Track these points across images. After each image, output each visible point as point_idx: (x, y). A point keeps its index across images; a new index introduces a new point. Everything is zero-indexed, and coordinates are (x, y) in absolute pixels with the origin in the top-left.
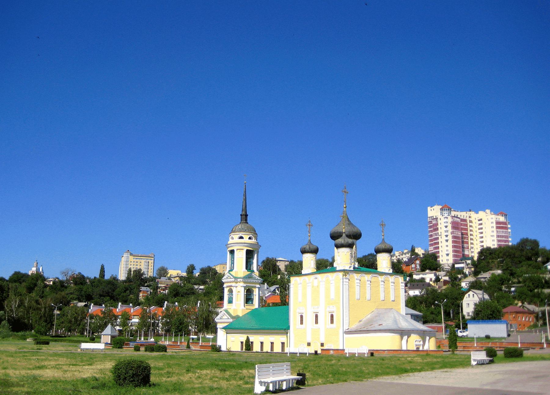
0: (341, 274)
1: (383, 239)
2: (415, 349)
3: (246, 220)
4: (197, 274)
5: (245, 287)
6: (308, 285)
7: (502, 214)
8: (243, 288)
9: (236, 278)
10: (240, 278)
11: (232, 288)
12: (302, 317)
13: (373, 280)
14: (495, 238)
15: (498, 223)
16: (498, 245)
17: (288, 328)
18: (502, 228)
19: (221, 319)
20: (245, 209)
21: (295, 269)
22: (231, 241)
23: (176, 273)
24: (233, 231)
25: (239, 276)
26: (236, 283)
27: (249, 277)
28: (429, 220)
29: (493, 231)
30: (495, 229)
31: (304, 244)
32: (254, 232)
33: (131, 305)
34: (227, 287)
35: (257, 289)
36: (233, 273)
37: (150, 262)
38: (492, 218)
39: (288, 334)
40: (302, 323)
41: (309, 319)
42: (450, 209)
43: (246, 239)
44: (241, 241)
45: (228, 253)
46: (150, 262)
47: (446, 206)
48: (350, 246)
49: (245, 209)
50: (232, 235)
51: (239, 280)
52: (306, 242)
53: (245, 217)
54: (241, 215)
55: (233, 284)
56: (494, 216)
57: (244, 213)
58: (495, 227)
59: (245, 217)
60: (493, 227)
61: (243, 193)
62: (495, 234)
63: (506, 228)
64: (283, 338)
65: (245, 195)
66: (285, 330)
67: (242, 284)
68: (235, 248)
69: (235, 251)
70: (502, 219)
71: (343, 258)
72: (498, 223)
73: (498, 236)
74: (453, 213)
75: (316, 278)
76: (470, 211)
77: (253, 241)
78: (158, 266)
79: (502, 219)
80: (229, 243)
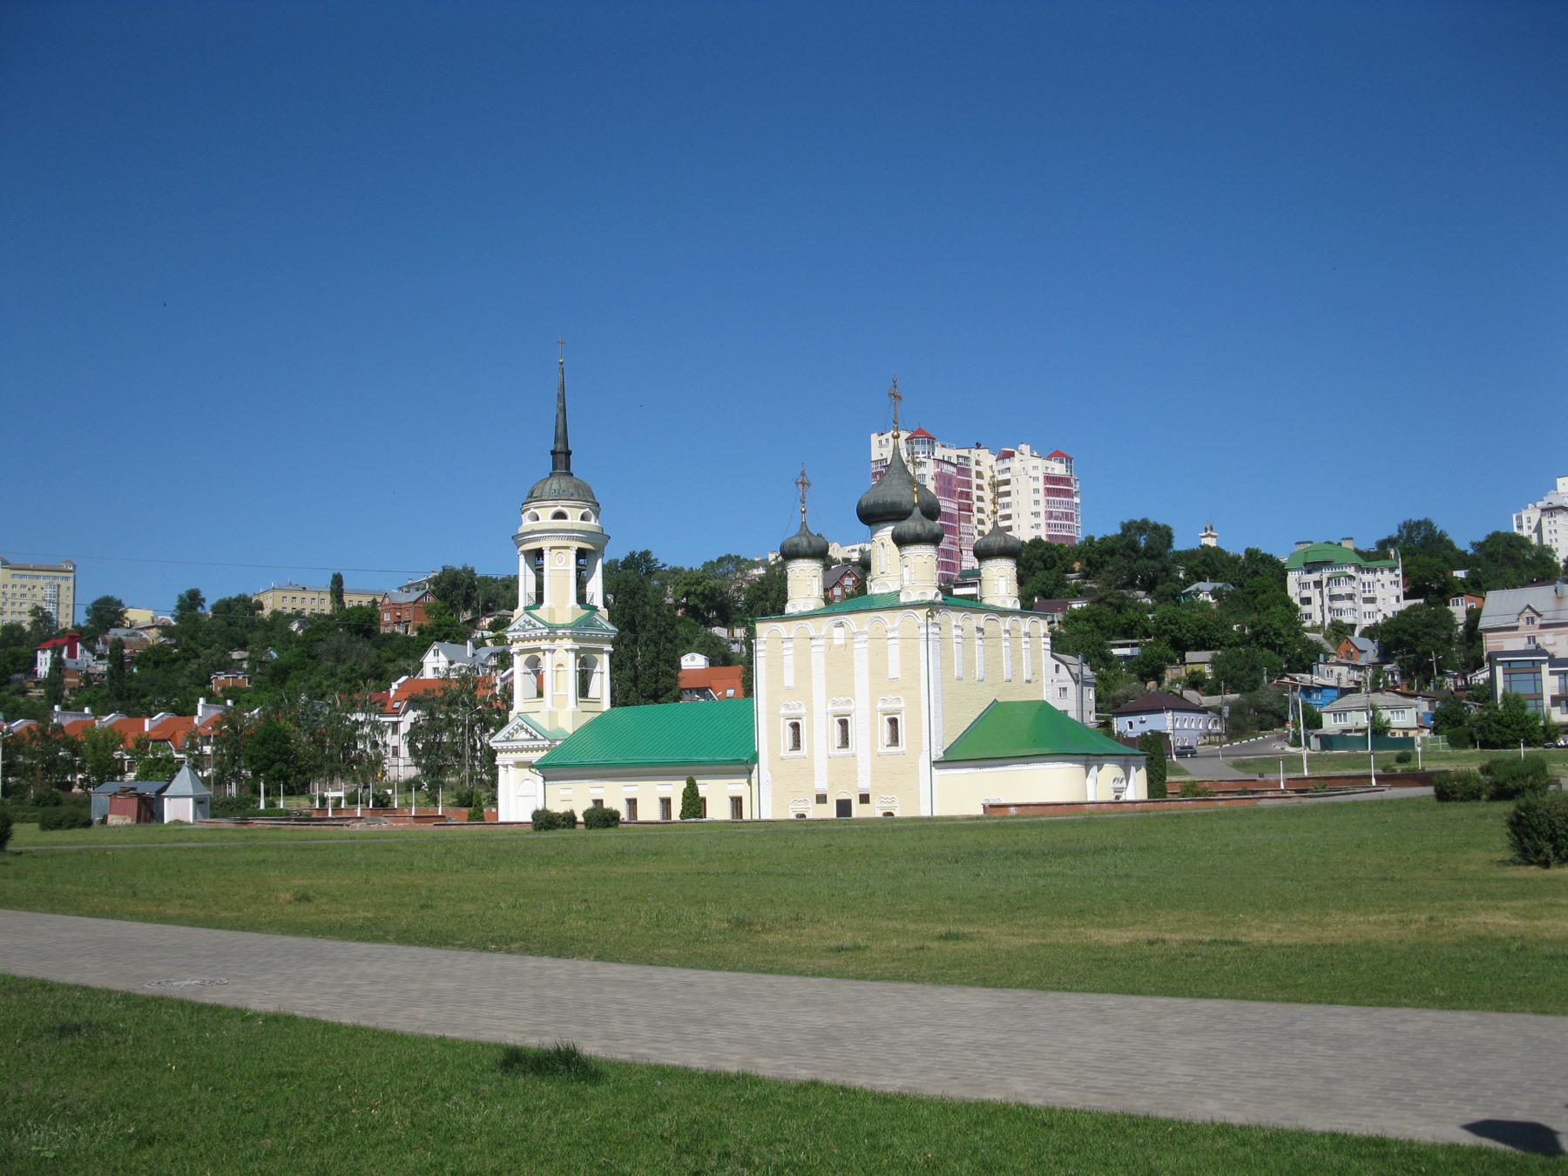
0: (921, 614)
1: (804, 524)
2: (1112, 798)
3: (568, 467)
4: (207, 610)
5: (577, 652)
6: (814, 642)
7: (1056, 455)
8: (572, 656)
9: (553, 628)
10: (564, 627)
11: (540, 655)
12: (796, 726)
13: (989, 628)
14: (1042, 520)
15: (1049, 479)
16: (1049, 536)
17: (755, 758)
18: (1058, 493)
19: (508, 740)
20: (562, 436)
21: (770, 599)
22: (527, 524)
23: (146, 616)
24: (532, 497)
25: (558, 621)
26: (553, 640)
27: (587, 623)
28: (874, 468)
29: (1037, 502)
30: (1041, 496)
31: (788, 532)
32: (584, 494)
33: (87, 710)
34: (522, 652)
35: (606, 658)
36: (541, 612)
37: (64, 584)
38: (1035, 468)
39: (755, 773)
40: (797, 744)
41: (822, 734)
42: (931, 440)
43: (574, 519)
44: (559, 523)
45: (522, 560)
46: (64, 584)
47: (920, 431)
48: (934, 540)
49: (562, 436)
50: (533, 508)
51: (560, 632)
52: (795, 529)
53: (562, 458)
54: (553, 453)
55: (544, 645)
56: (1039, 462)
57: (560, 447)
58: (1042, 491)
59: (562, 458)
60: (1036, 491)
61: (556, 391)
62: (1042, 508)
63: (1068, 494)
64: (737, 787)
65: (562, 397)
66: (744, 764)
67: (568, 644)
68: (544, 544)
69: (546, 552)
70: (1059, 469)
71: (904, 570)
72: (1049, 479)
73: (1050, 515)
74: (940, 452)
75: (841, 625)
76: (978, 446)
77: (593, 524)
78: (89, 599)
79: (1059, 469)
80: (521, 531)
